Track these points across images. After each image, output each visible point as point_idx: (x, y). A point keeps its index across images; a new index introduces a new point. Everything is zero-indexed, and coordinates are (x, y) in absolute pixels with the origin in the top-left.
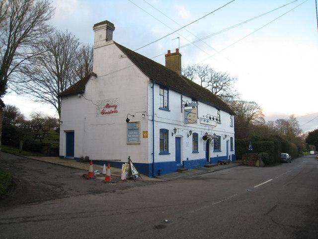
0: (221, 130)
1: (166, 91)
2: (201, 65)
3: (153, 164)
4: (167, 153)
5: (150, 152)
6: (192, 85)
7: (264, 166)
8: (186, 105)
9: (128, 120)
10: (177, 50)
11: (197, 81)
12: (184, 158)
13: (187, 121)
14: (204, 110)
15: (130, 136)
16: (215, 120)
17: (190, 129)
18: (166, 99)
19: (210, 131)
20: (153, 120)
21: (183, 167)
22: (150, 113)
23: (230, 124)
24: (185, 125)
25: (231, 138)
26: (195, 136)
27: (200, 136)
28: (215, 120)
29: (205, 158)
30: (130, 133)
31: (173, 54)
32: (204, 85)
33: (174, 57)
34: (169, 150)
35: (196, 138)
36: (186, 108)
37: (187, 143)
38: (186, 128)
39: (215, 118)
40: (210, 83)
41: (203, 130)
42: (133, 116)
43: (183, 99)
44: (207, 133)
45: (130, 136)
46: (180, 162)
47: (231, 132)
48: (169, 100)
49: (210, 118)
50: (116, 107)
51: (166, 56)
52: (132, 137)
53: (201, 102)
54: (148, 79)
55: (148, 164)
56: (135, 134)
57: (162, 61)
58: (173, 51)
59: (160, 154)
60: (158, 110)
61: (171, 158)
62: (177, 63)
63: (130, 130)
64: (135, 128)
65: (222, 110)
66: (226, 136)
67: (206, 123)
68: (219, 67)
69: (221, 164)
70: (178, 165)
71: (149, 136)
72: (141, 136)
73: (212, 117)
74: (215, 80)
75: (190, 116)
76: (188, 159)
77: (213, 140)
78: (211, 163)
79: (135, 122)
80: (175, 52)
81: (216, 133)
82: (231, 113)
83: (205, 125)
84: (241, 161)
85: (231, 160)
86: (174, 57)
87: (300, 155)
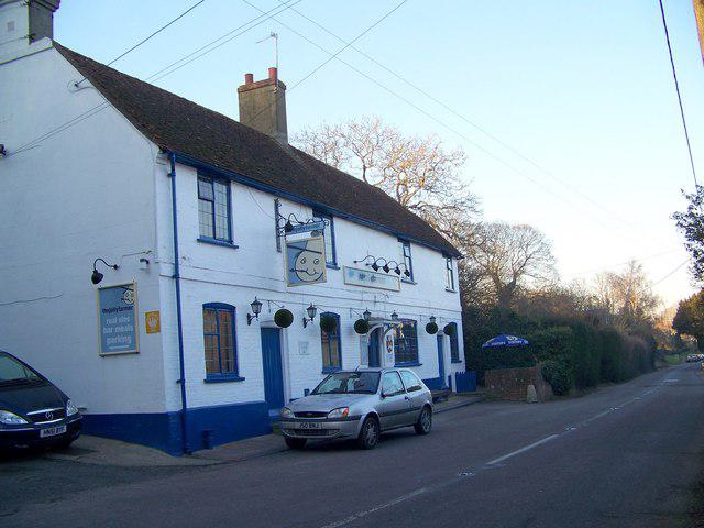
2: (359, 122)
3: (184, 414)
5: (171, 375)
6: (312, 165)
7: (551, 400)
8: (289, 228)
9: (97, 278)
10: (274, 71)
11: (351, 167)
13: (295, 276)
14: (355, 242)
15: (110, 331)
16: (392, 272)
17: (309, 301)
18: (221, 210)
19: (380, 307)
20: (176, 277)
23: (445, 283)
24: (292, 289)
26: (330, 324)
27: (347, 322)
28: (392, 272)
29: (263, 400)
30: (109, 321)
33: (266, 95)
36: (292, 238)
37: (304, 346)
39: (392, 266)
40: (389, 172)
41: (355, 305)
42: (116, 267)
44: (367, 313)
45: (110, 331)
48: (177, 202)
49: (375, 267)
51: (242, 90)
52: (114, 335)
53: (345, 218)
54: (156, 149)
55: (166, 415)
56: (125, 324)
57: (229, 107)
58: (261, 75)
59: (206, 382)
61: (250, 389)
62: (273, 108)
63: (110, 311)
64: (122, 305)
67: (368, 283)
68: (411, 125)
70: (273, 413)
71: (163, 327)
72: (142, 328)
73: (381, 264)
74: (404, 158)
75: (304, 261)
79: (122, 287)
80: (266, 76)
82: (448, 252)
83: (360, 289)
86: (266, 95)
87: (657, 364)
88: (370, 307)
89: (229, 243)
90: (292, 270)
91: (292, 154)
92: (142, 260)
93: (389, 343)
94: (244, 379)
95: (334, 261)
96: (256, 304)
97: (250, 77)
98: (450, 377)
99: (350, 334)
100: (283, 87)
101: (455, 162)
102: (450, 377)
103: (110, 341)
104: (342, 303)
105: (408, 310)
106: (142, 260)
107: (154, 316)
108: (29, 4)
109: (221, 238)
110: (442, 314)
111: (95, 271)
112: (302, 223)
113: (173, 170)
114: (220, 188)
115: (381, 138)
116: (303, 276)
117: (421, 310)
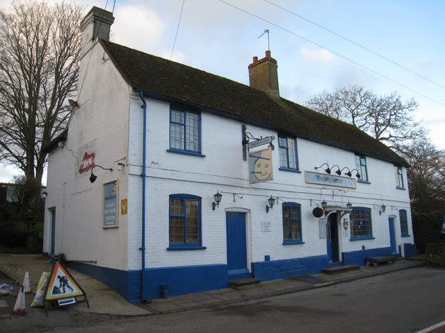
0: (373, 197)
1: (290, 141)
2: (347, 89)
4: (198, 246)
10: (268, 53)
12: (146, 267)
14: (313, 155)
17: (270, 194)
20: (143, 176)
21: (252, 275)
22: (134, 158)
24: (254, 185)
25: (403, 212)
27: (306, 209)
31: (264, 60)
32: (359, 122)
33: (265, 68)
34: (203, 241)
35: (404, 215)
37: (266, 227)
38: (260, 192)
41: (313, 197)
42: (111, 170)
43: (131, 106)
46: (245, 266)
47: (403, 200)
50: (94, 157)
51: (251, 67)
54: (131, 89)
58: (261, 56)
60: (279, 171)
61: (214, 252)
65: (308, 138)
66: (384, 207)
69: (371, 265)
75: (259, 165)
76: (267, 258)
77: (347, 216)
78: (343, 263)
81: (351, 201)
82: (398, 163)
83: (321, 187)
84: (422, 257)
85: (403, 254)
88: (327, 199)
89: (199, 154)
90: (252, 173)
91: (282, 105)
92: (119, 164)
93: (345, 223)
94: (205, 248)
95: (297, 167)
96: (218, 196)
97: (255, 58)
98: (400, 247)
99: (309, 217)
100: (274, 62)
101: (410, 109)
102: (400, 247)
103: (107, 219)
104: (303, 196)
105: (359, 201)
106: (119, 164)
107: (125, 202)
108: (94, 22)
109: (291, 168)
110: (282, 194)
111: (92, 175)
112: (258, 140)
113: (144, 102)
114: (190, 118)
115: (363, 99)
116: (259, 176)
117: (375, 202)
